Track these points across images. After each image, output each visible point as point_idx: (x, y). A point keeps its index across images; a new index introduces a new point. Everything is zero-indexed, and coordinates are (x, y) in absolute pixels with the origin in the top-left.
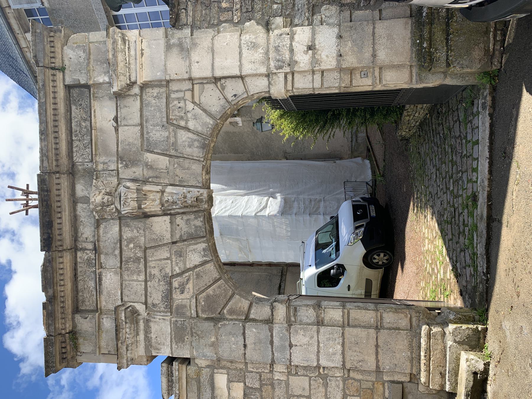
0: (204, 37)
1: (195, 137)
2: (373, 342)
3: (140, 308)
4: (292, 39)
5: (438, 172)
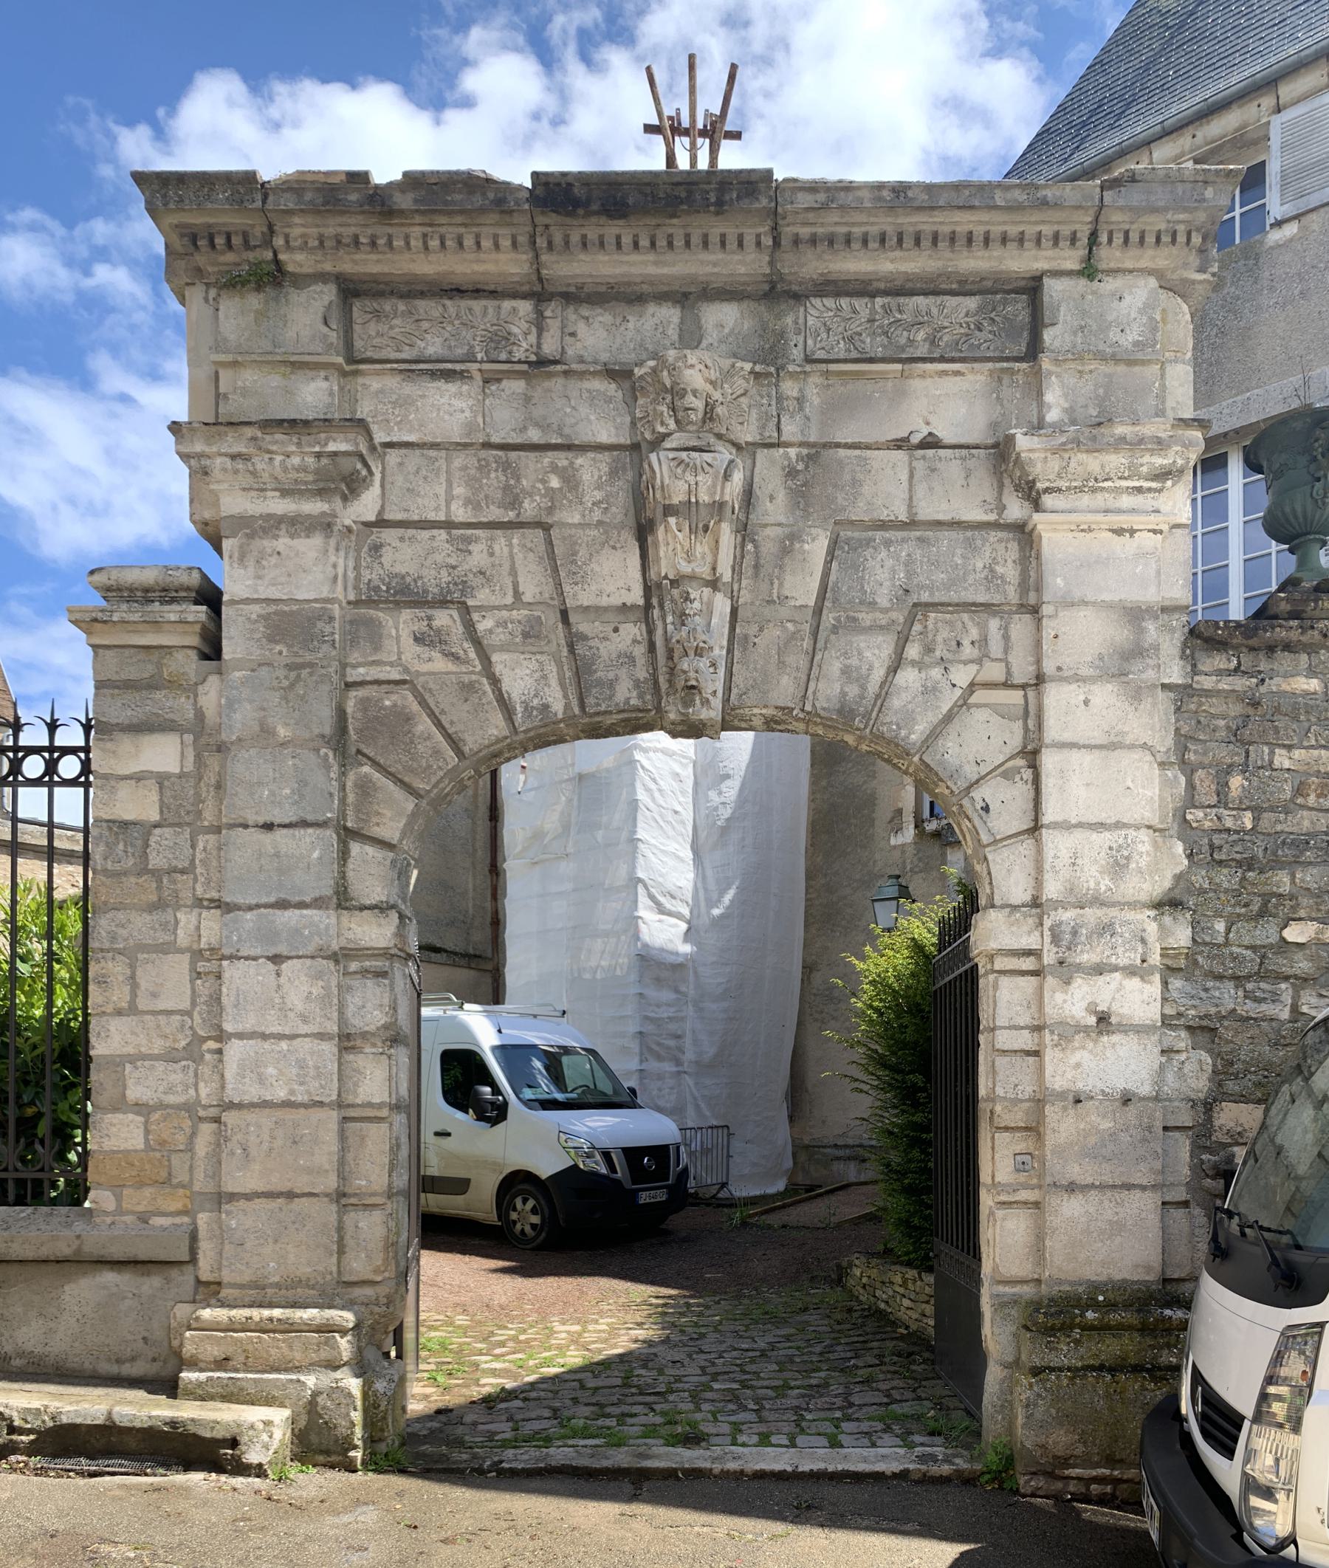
0: (1151, 724)
1: (873, 687)
2: (301, 1184)
3: (367, 505)
4: (1130, 971)
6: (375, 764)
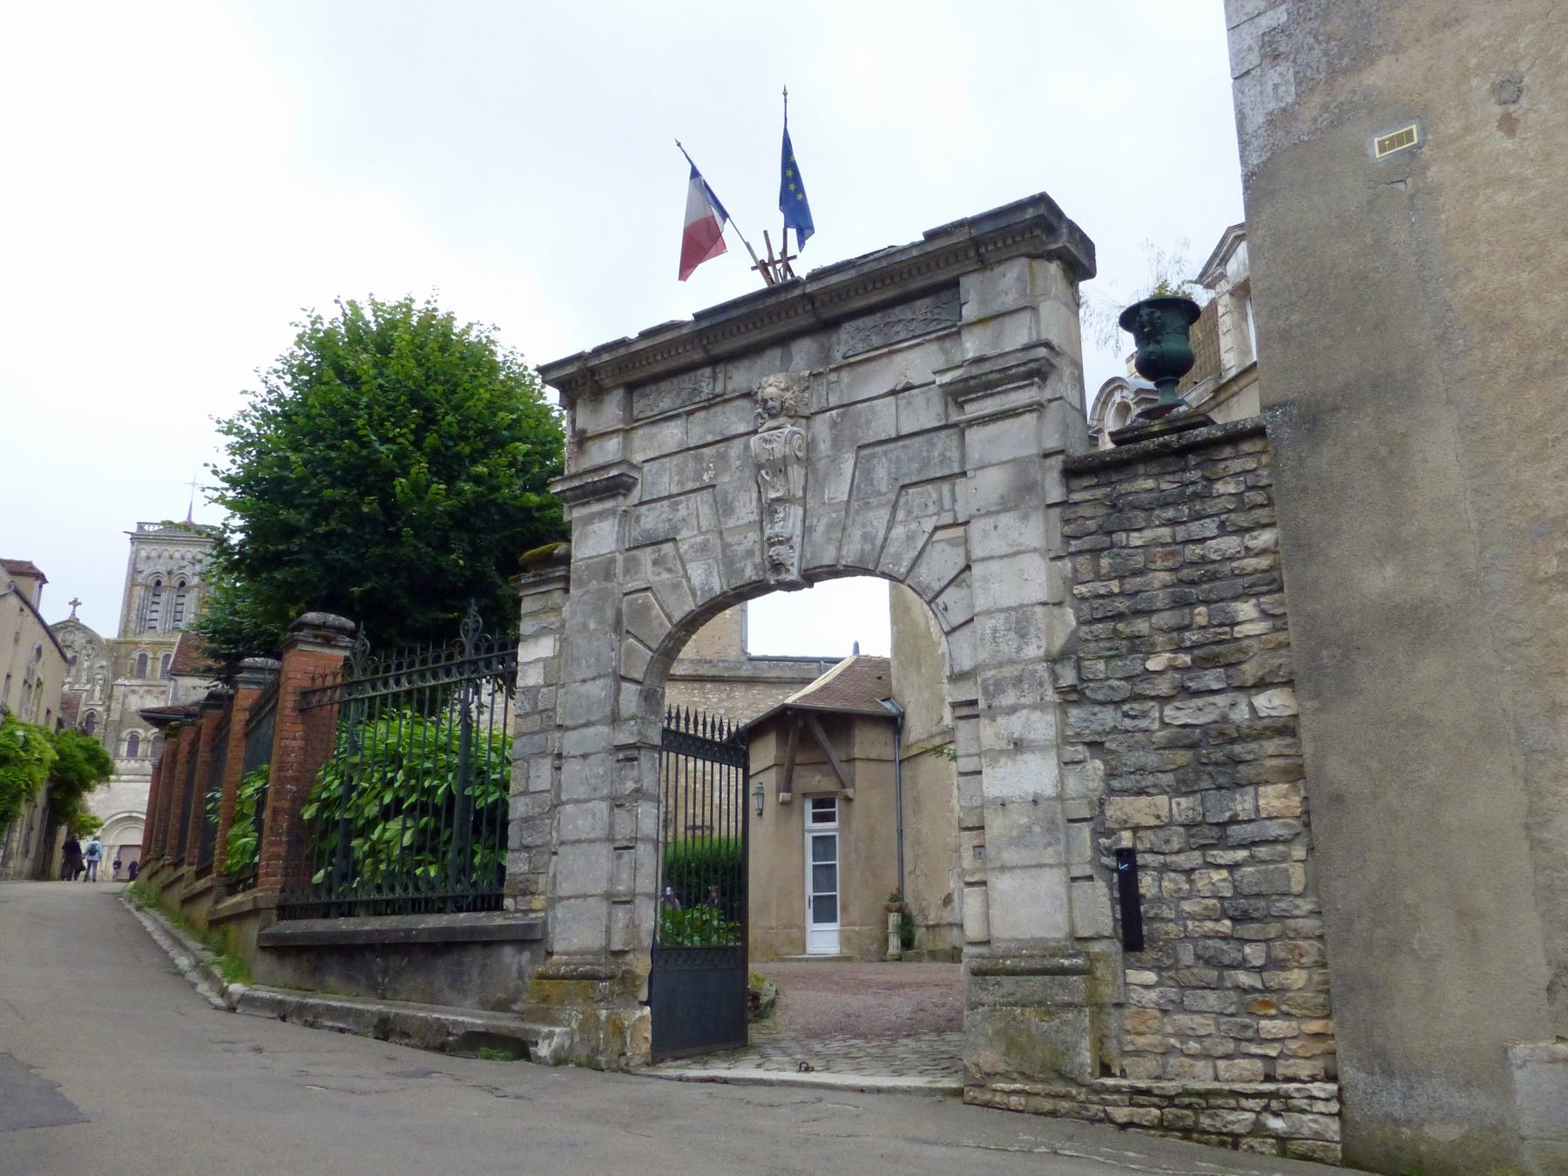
0: (1033, 531)
1: (879, 542)
4: (1034, 707)
5: (1176, 1101)
6: (635, 637)
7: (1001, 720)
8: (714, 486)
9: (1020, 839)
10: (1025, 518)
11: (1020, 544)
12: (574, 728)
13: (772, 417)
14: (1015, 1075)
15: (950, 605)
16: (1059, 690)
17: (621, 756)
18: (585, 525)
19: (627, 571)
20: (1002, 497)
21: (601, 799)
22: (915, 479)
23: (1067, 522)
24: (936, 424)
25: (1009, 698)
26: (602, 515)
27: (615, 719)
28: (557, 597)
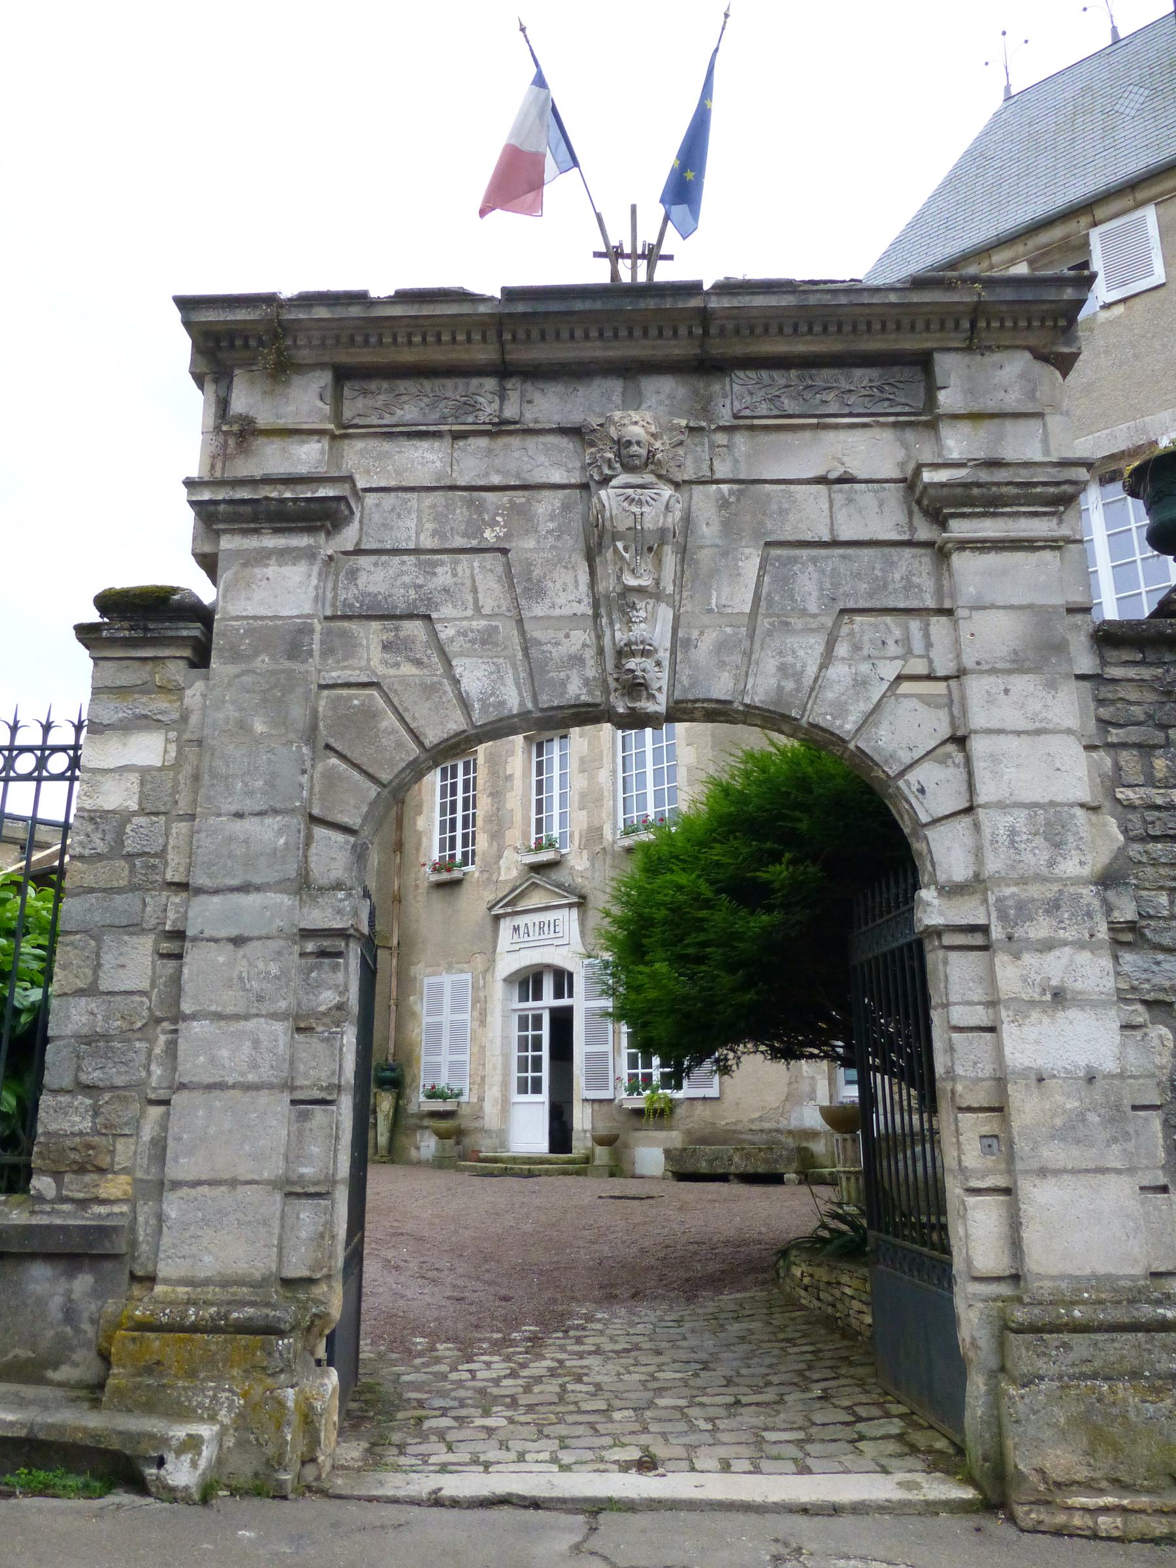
0: (1067, 707)
1: (808, 681)
4: (1080, 945)
7: (1028, 958)
8: (504, 551)
9: (1070, 1130)
10: (1051, 685)
11: (1049, 721)
12: (216, 892)
13: (629, 468)
14: (1104, 1484)
15: (930, 787)
16: (1113, 927)
17: (310, 947)
18: (245, 565)
19: (328, 651)
20: (1015, 652)
21: (274, 1016)
22: (862, 604)
23: (1101, 702)
24: (894, 536)
25: (1040, 929)
26: (284, 555)
27: (304, 886)
28: (176, 671)
